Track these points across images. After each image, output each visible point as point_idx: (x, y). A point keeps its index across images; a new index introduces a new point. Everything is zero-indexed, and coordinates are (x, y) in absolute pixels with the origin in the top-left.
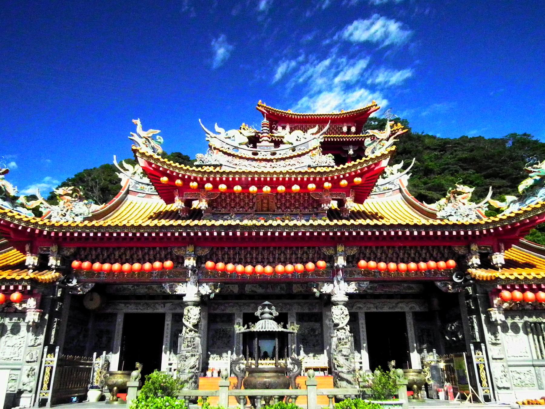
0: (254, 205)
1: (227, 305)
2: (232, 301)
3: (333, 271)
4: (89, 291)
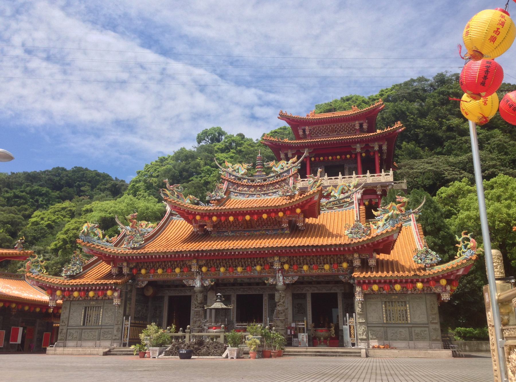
4: (145, 286)
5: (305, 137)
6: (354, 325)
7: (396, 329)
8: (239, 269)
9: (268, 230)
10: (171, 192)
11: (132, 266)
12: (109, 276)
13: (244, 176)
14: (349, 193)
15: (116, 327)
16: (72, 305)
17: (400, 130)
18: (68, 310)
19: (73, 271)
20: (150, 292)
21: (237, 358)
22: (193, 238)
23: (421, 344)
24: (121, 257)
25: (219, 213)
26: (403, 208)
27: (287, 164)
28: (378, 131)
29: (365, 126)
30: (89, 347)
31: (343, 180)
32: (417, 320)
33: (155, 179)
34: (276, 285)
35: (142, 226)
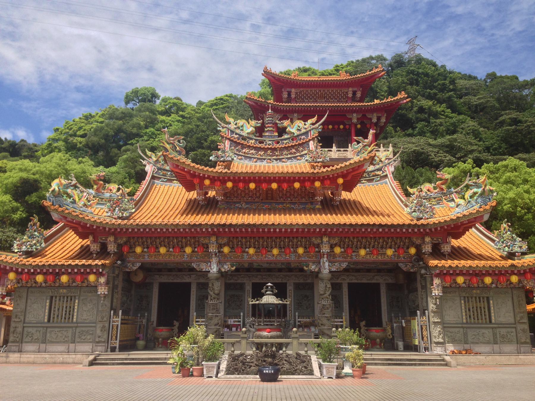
0: (260, 194)
1: (239, 276)
2: (243, 273)
3: (321, 254)
5: (289, 100)
6: (427, 325)
7: (478, 330)
8: (275, 251)
9: (294, 203)
10: (171, 146)
11: (120, 241)
12: (84, 253)
13: (251, 136)
14: (381, 165)
15: (99, 325)
16: (29, 294)
17: (405, 101)
18: (24, 301)
19: (31, 246)
20: (139, 278)
21: (336, 378)
22: (193, 207)
23: (508, 348)
24: (110, 229)
25: (237, 178)
26: (444, 187)
27: (305, 125)
28: (376, 101)
29: (359, 95)
30: (57, 352)
31: (338, 153)
32: (502, 320)
33: (80, 139)
34: (319, 272)
35: (111, 190)
